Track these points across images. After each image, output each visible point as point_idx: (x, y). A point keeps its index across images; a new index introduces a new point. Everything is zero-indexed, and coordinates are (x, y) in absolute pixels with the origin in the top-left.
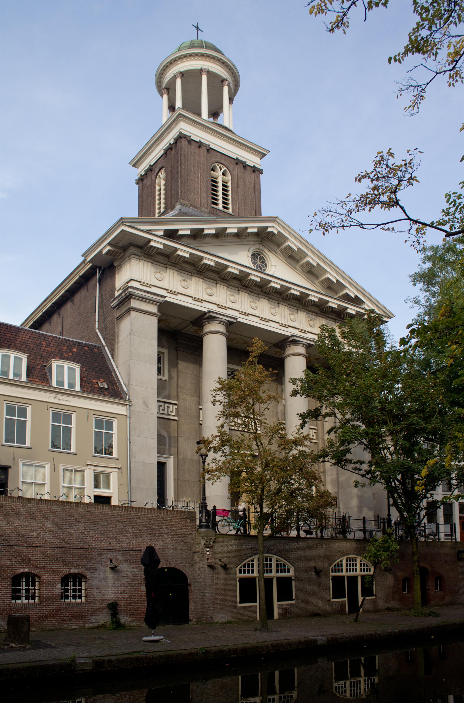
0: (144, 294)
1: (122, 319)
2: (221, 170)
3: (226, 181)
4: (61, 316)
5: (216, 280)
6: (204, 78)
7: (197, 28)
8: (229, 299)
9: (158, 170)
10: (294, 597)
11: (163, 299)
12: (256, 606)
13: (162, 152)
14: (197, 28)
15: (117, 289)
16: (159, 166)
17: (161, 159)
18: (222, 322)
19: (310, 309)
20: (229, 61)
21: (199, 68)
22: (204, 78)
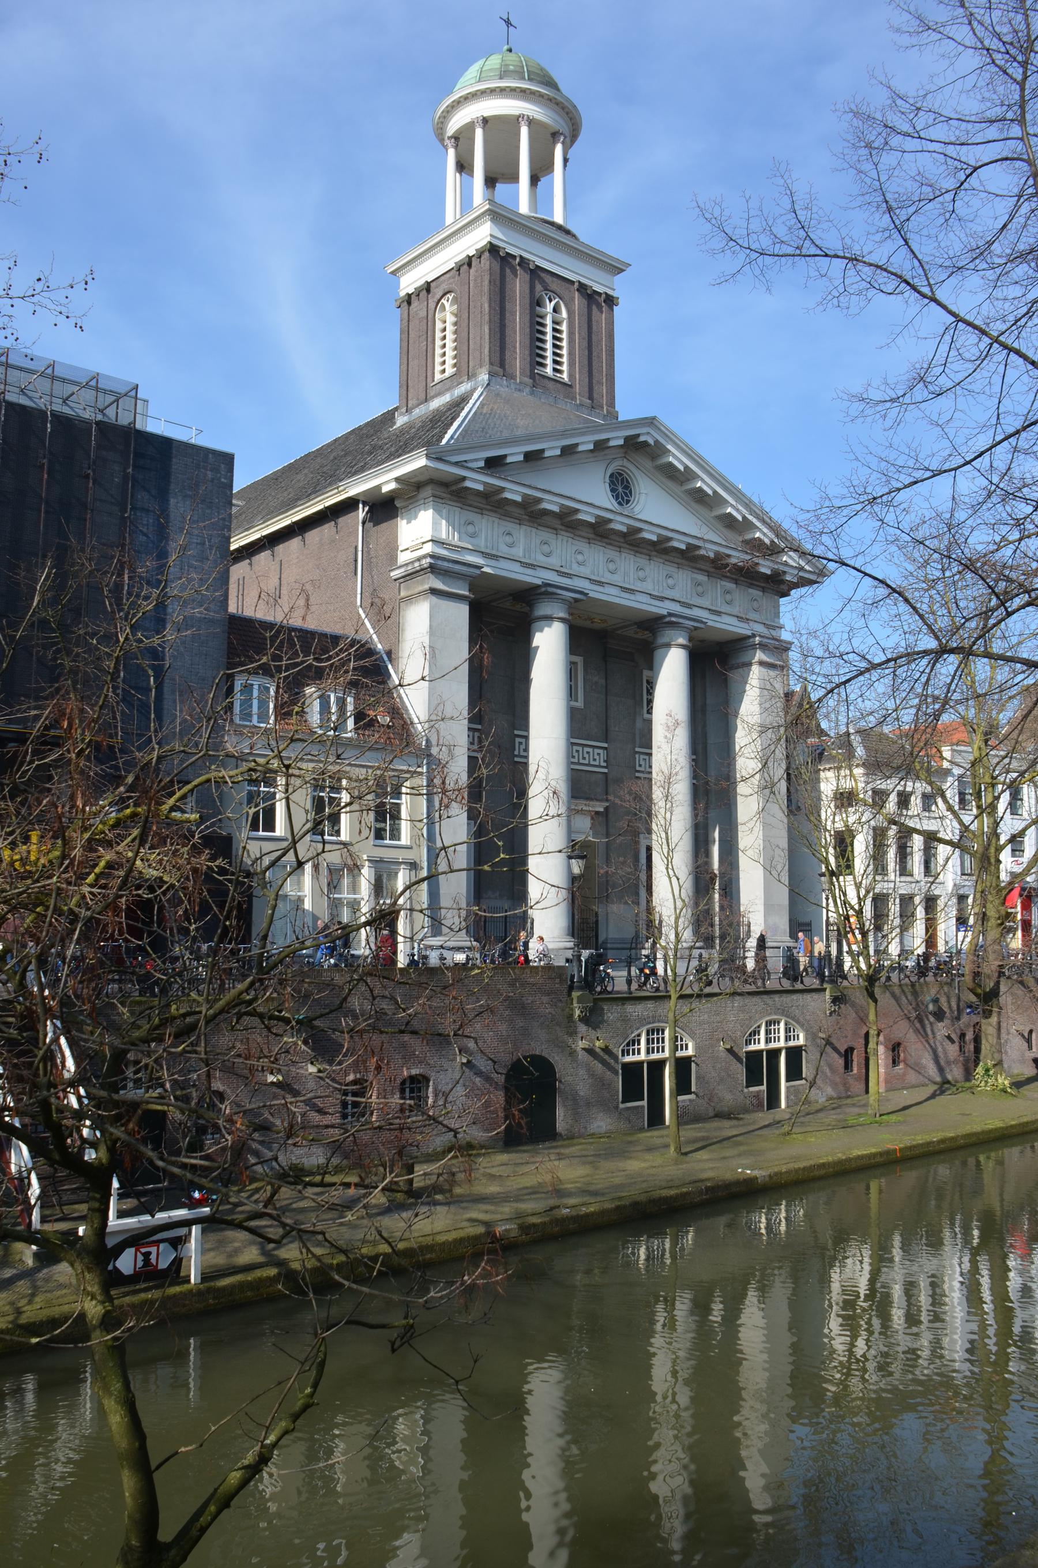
0: (450, 565)
1: (411, 603)
2: (550, 301)
3: (559, 320)
4: (277, 559)
5: (556, 529)
6: (524, 131)
7: (508, 23)
8: (576, 558)
9: (441, 294)
10: (693, 1089)
11: (478, 572)
12: (643, 1107)
13: (451, 265)
14: (508, 23)
15: (401, 548)
16: (444, 287)
17: (448, 275)
18: (564, 601)
19: (698, 566)
20: (568, 100)
21: (517, 113)
22: (524, 131)
